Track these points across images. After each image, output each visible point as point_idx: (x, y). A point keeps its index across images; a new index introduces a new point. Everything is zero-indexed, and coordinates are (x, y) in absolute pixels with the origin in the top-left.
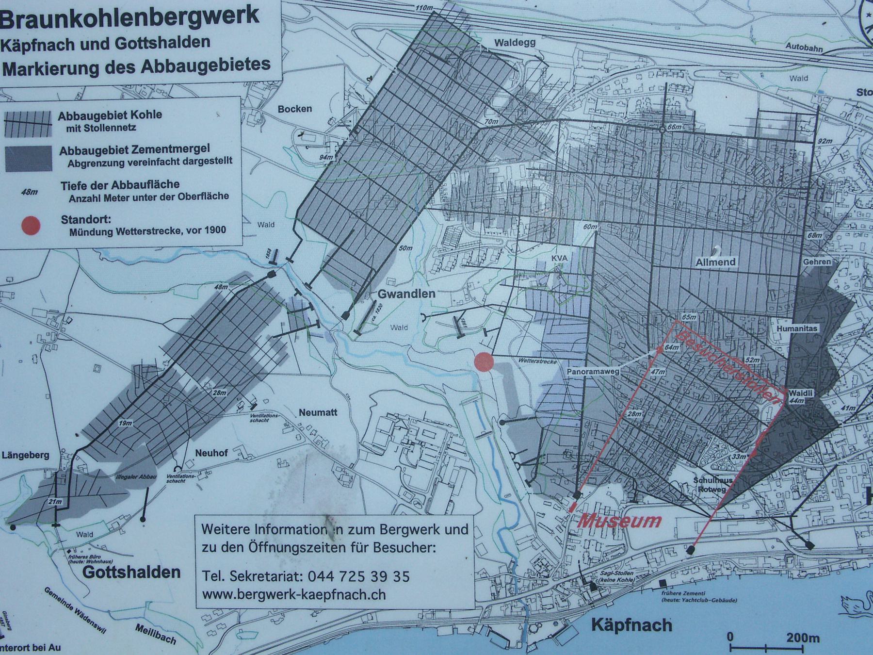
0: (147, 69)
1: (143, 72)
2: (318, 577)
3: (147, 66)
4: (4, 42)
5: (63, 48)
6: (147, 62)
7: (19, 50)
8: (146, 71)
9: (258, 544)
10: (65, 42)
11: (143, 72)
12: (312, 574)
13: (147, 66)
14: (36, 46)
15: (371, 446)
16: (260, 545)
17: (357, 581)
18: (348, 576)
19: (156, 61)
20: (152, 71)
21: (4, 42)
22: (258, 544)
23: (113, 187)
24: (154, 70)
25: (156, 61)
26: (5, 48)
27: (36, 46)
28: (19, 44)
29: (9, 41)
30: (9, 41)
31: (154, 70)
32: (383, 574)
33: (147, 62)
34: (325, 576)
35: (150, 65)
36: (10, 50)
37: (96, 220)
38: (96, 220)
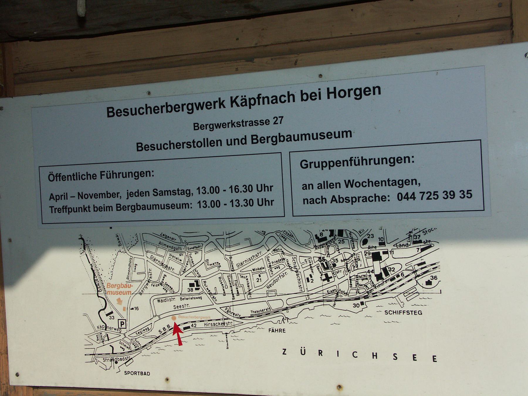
0: (334, 201)
1: (331, 202)
2: (404, 198)
3: (334, 199)
4: (233, 99)
5: (285, 101)
6: (334, 196)
7: (246, 105)
8: (333, 202)
9: (55, 175)
10: (287, 95)
11: (331, 202)
12: (400, 195)
13: (334, 199)
14: (261, 100)
15: (131, 356)
16: (56, 176)
17: (433, 199)
18: (426, 196)
19: (339, 196)
20: (337, 202)
21: (233, 99)
22: (55, 175)
23: (332, 201)
24: (338, 202)
25: (339, 196)
26: (234, 104)
27: (261, 100)
28: (246, 100)
29: (237, 97)
30: (237, 97)
31: (338, 202)
32: (452, 193)
33: (334, 196)
34: (409, 197)
35: (335, 198)
36: (238, 106)
37: (342, 94)
38: (342, 94)
